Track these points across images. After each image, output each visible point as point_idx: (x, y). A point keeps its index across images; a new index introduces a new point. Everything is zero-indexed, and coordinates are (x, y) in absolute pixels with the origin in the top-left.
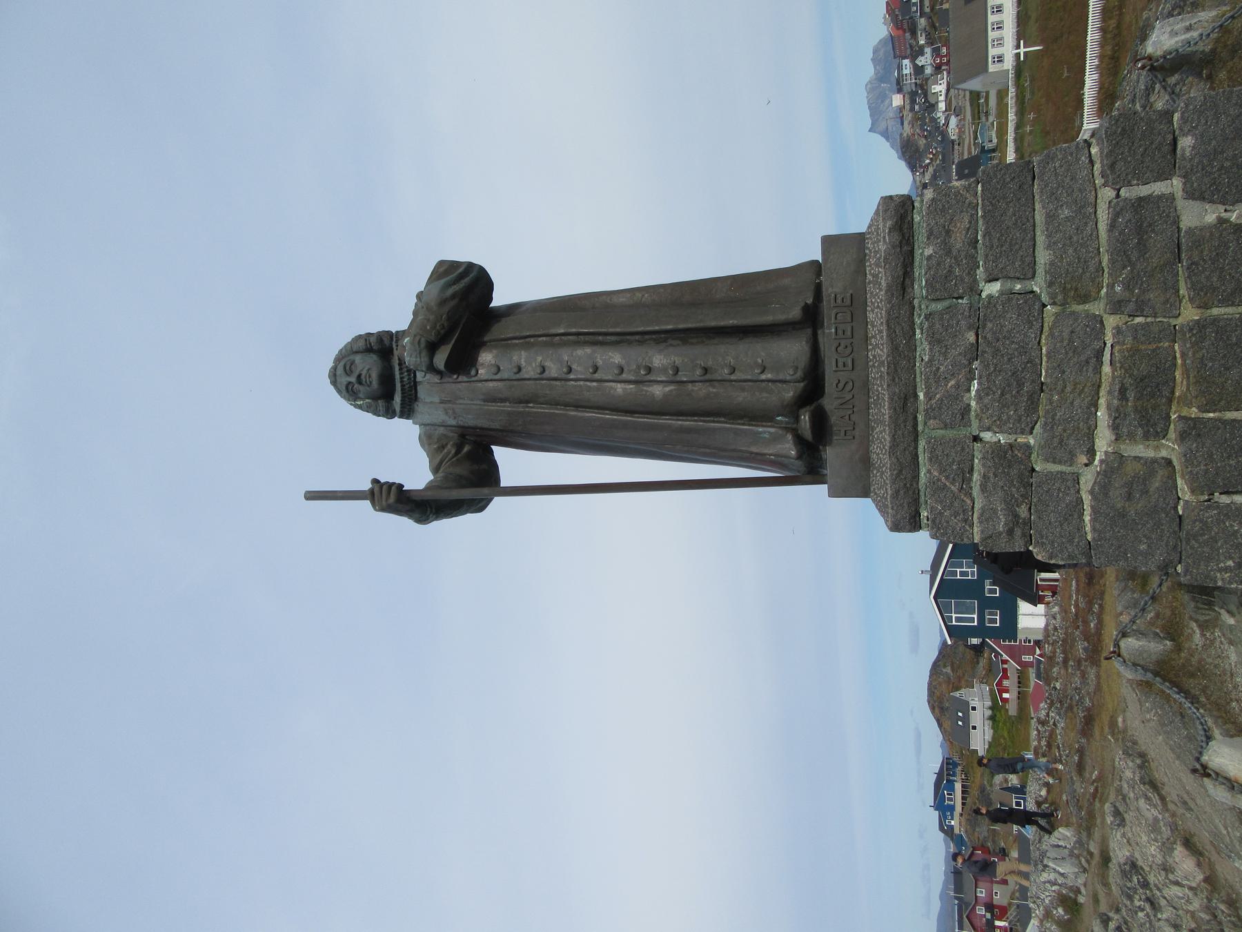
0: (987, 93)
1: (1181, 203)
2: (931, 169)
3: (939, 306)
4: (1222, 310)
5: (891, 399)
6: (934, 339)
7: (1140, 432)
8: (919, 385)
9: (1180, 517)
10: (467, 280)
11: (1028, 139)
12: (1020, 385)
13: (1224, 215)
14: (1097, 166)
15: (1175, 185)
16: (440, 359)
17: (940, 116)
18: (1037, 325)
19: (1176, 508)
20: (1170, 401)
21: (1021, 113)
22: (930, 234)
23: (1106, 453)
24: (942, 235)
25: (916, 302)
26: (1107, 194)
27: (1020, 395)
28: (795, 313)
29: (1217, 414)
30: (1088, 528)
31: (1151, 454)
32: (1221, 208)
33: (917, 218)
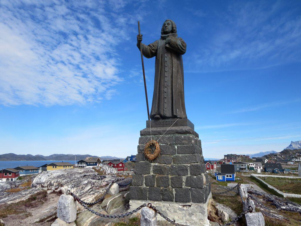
0: (297, 172)
2: (281, 157)
5: (160, 131)
6: (169, 138)
7: (154, 169)
11: (285, 181)
15: (189, 175)
16: (167, 46)
17: (294, 160)
21: (291, 179)
24: (185, 139)
26: (189, 165)
28: (175, 114)
33: (188, 135)
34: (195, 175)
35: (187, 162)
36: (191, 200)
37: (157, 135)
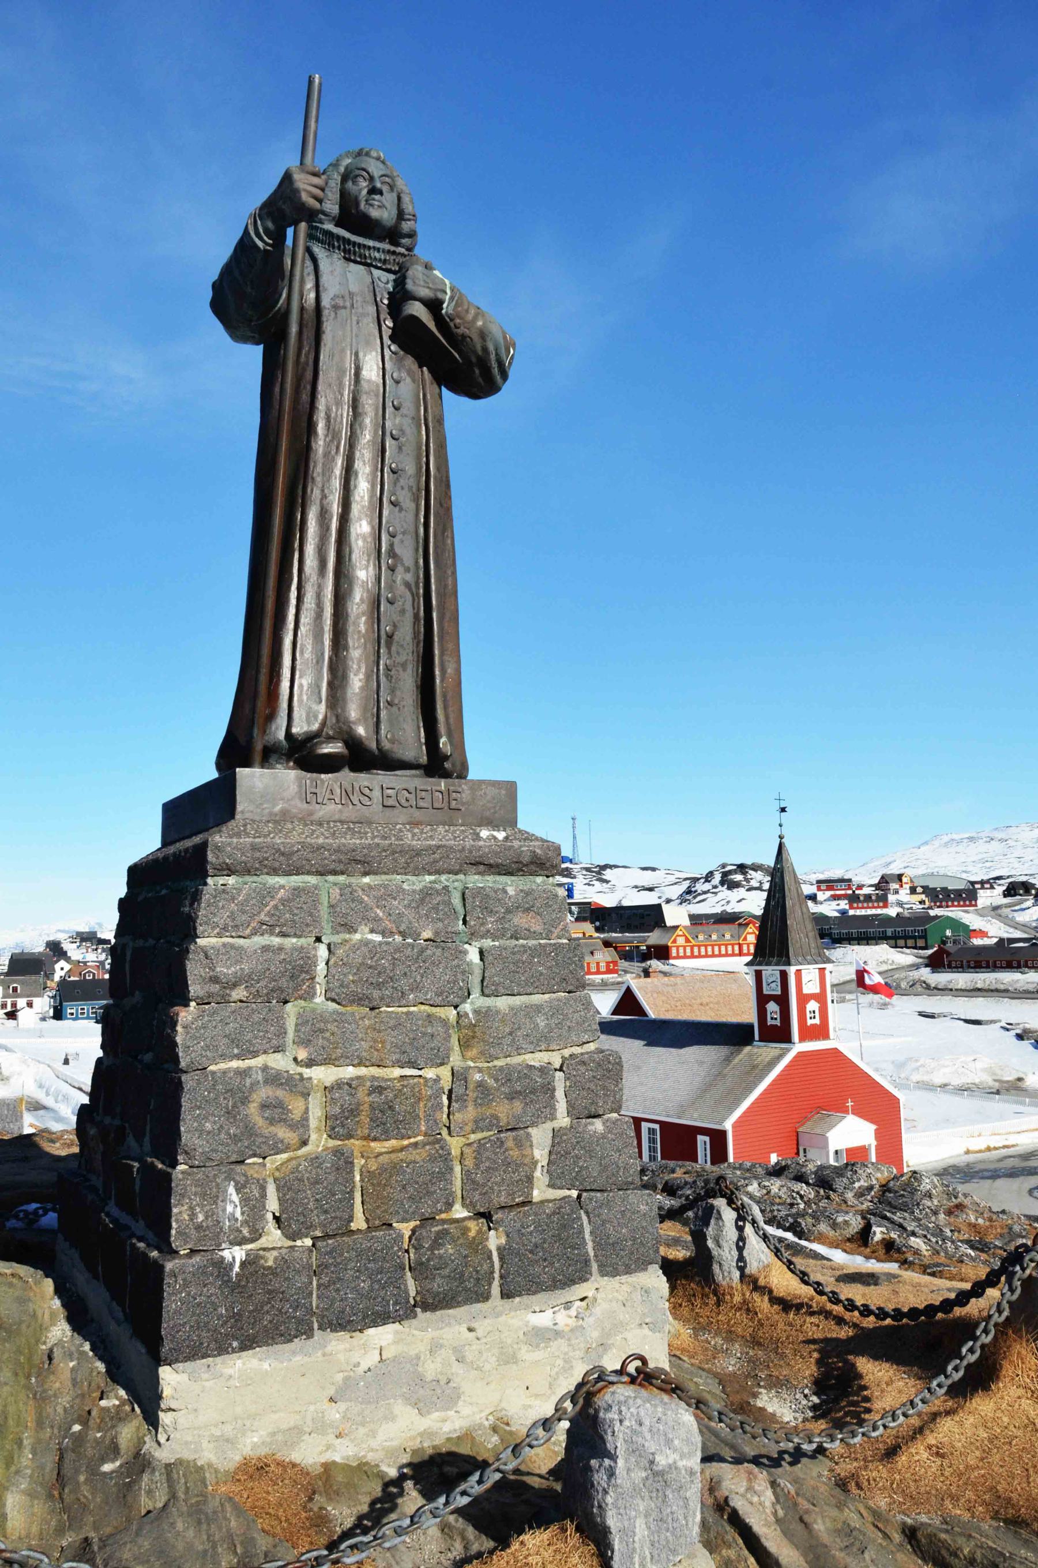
1: (549, 1126)
3: (456, 901)
4: (459, 1175)
6: (426, 893)
8: (378, 877)
9: (243, 1162)
10: (496, 371)
12: (379, 986)
13: (540, 1165)
14: (577, 1050)
15: (563, 1120)
18: (438, 1000)
19: (254, 1155)
20: (366, 1138)
22: (528, 893)
23: (310, 1078)
24: (527, 904)
25: (461, 877)
27: (367, 987)
29: (358, 1184)
30: (223, 1066)
31: (313, 1123)
32: (545, 1163)
33: (539, 880)
34: (594, 1117)
35: (542, 1041)
36: (595, 1267)
37: (334, 873)
